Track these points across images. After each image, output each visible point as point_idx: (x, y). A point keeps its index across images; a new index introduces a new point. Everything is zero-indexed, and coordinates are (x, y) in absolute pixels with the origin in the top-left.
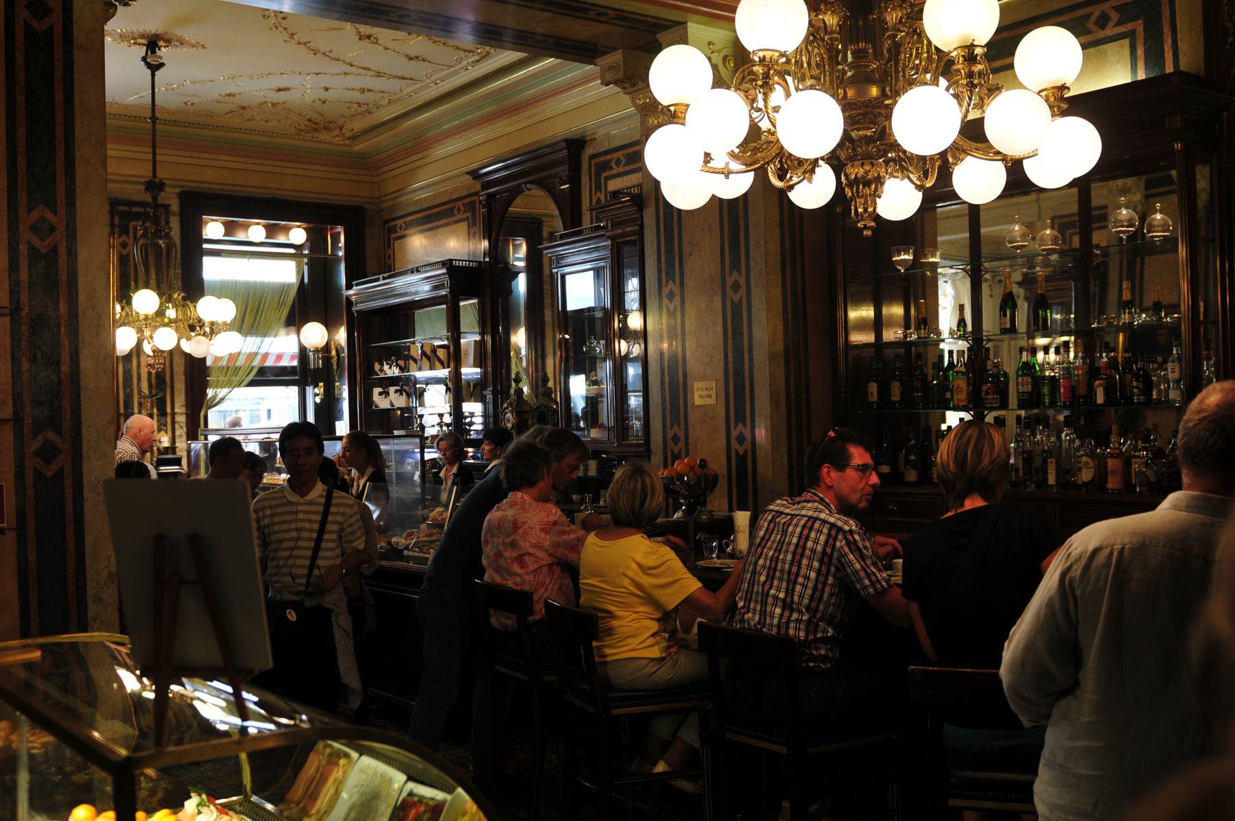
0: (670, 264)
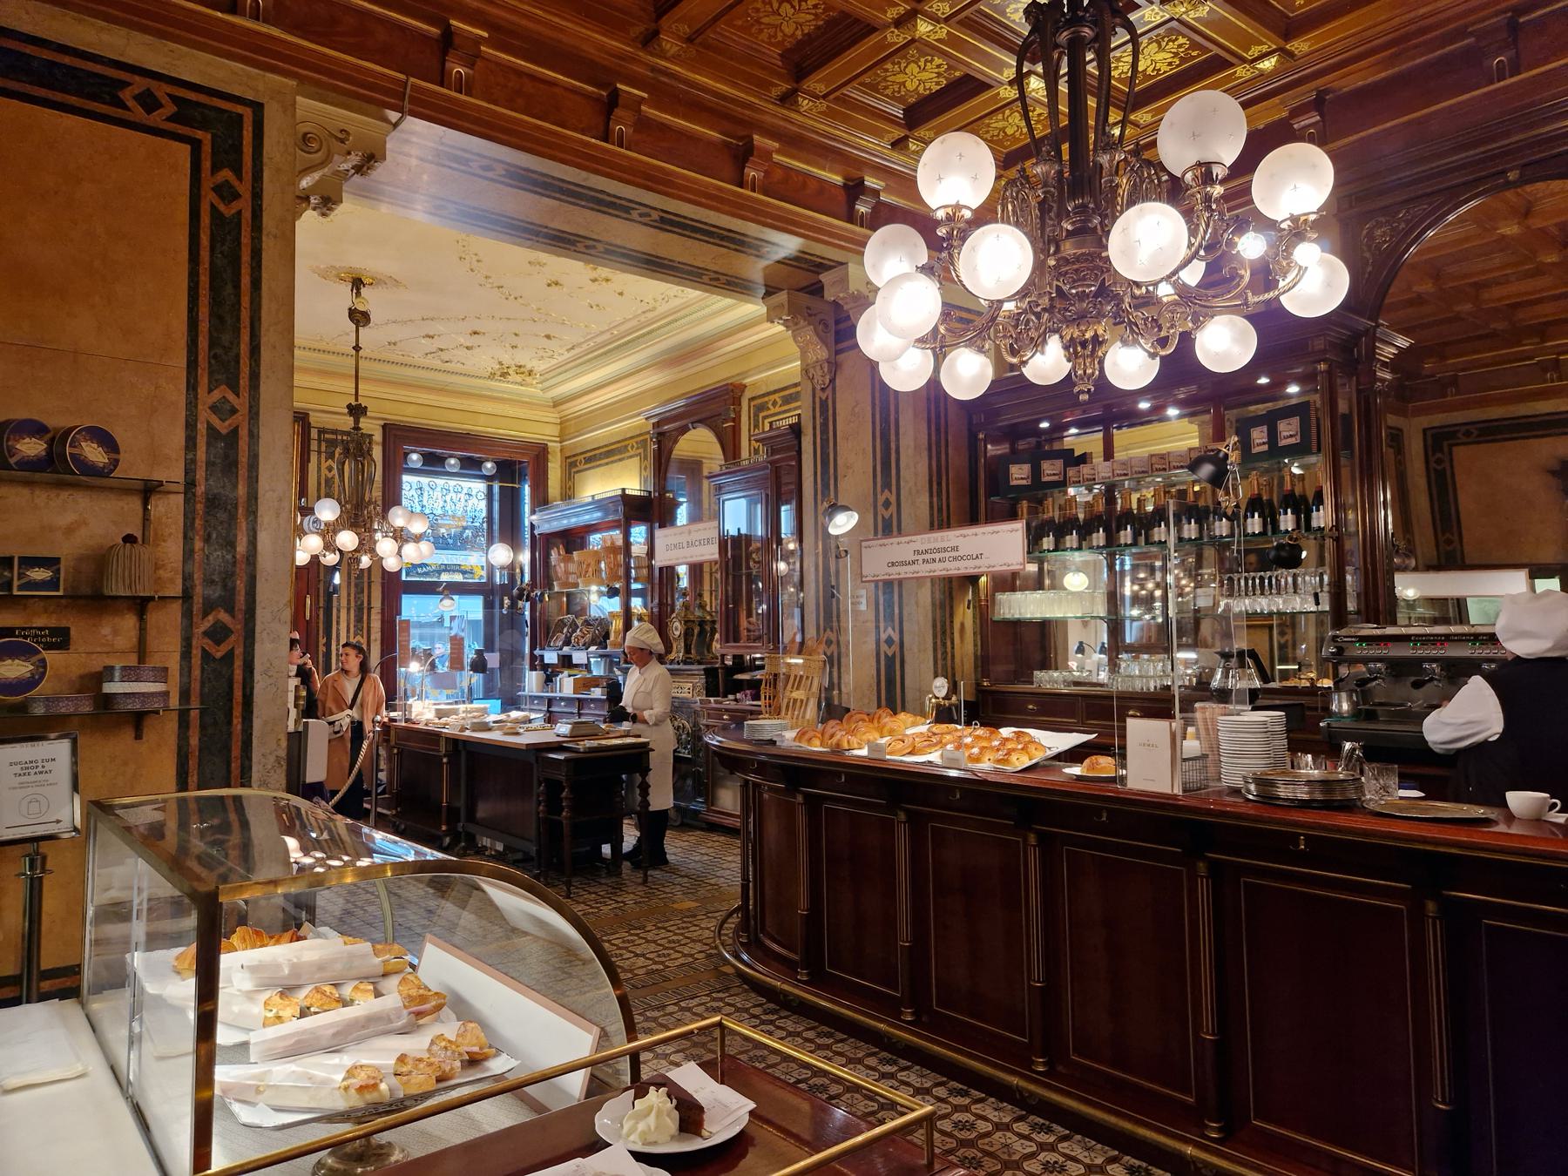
0: (826, 486)
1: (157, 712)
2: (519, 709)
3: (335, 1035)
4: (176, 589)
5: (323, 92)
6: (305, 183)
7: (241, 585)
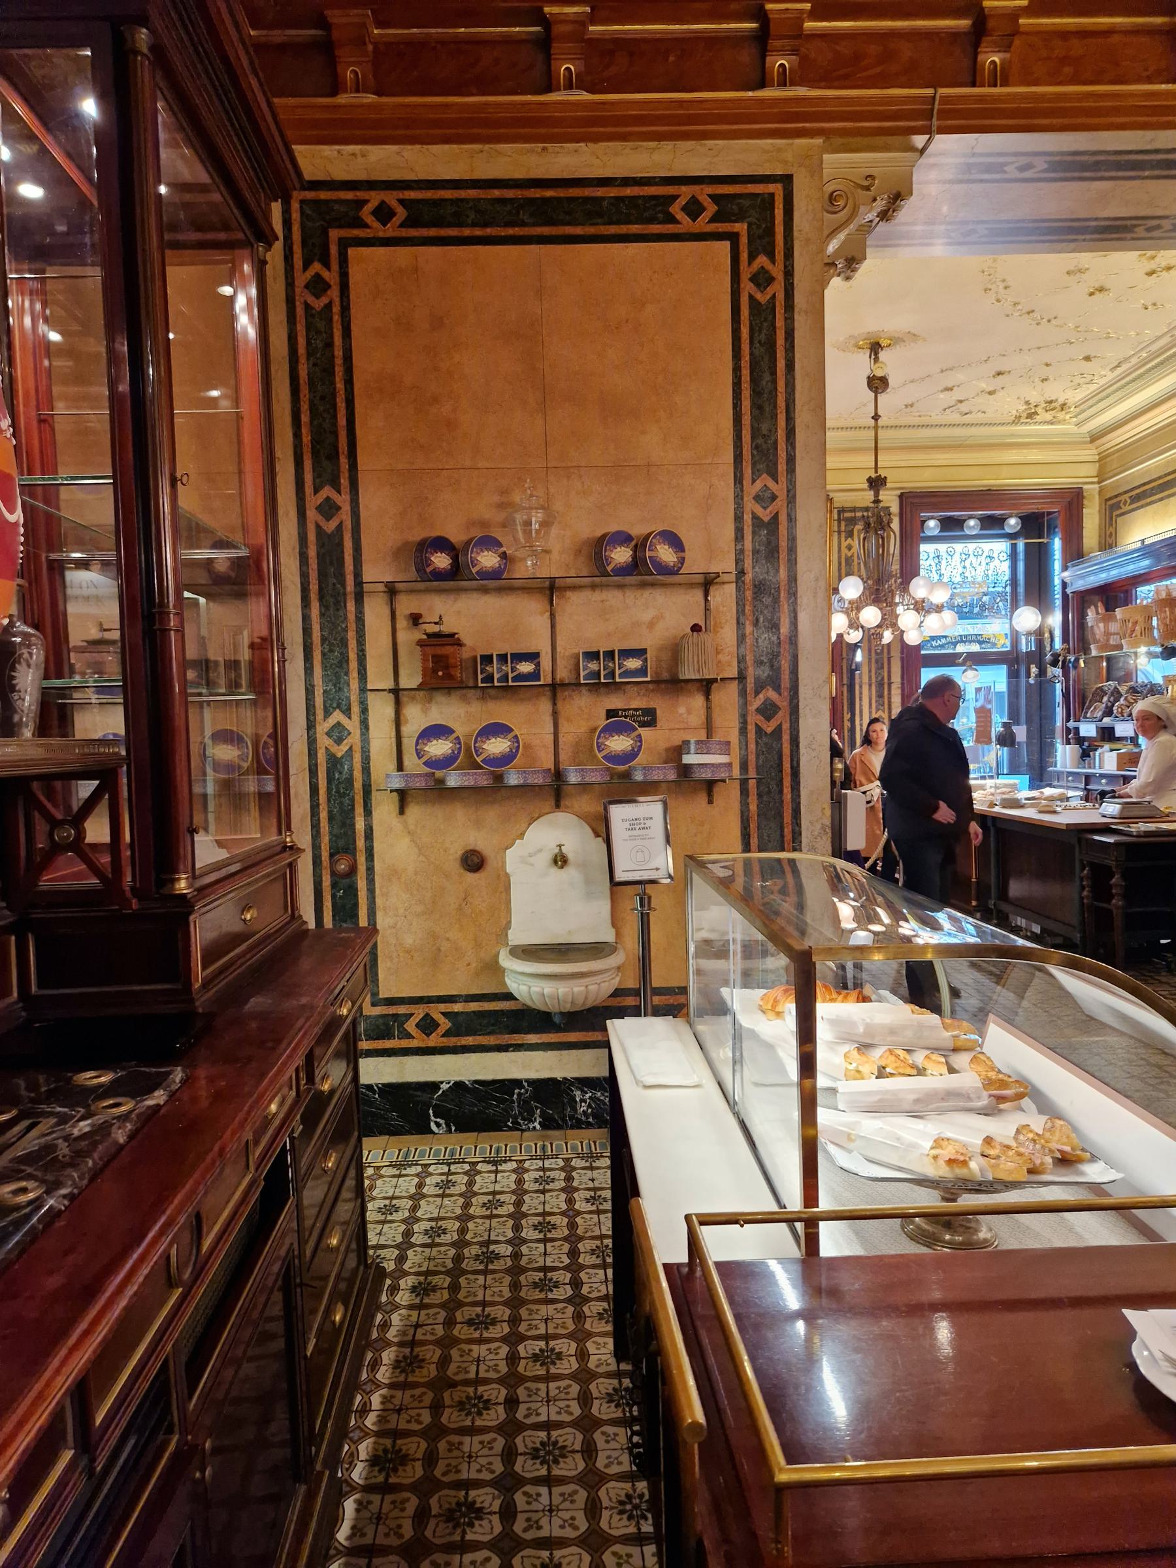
1: (724, 781)
2: (1050, 786)
3: (917, 1101)
4: (733, 672)
5: (849, 140)
6: (832, 247)
7: (785, 665)
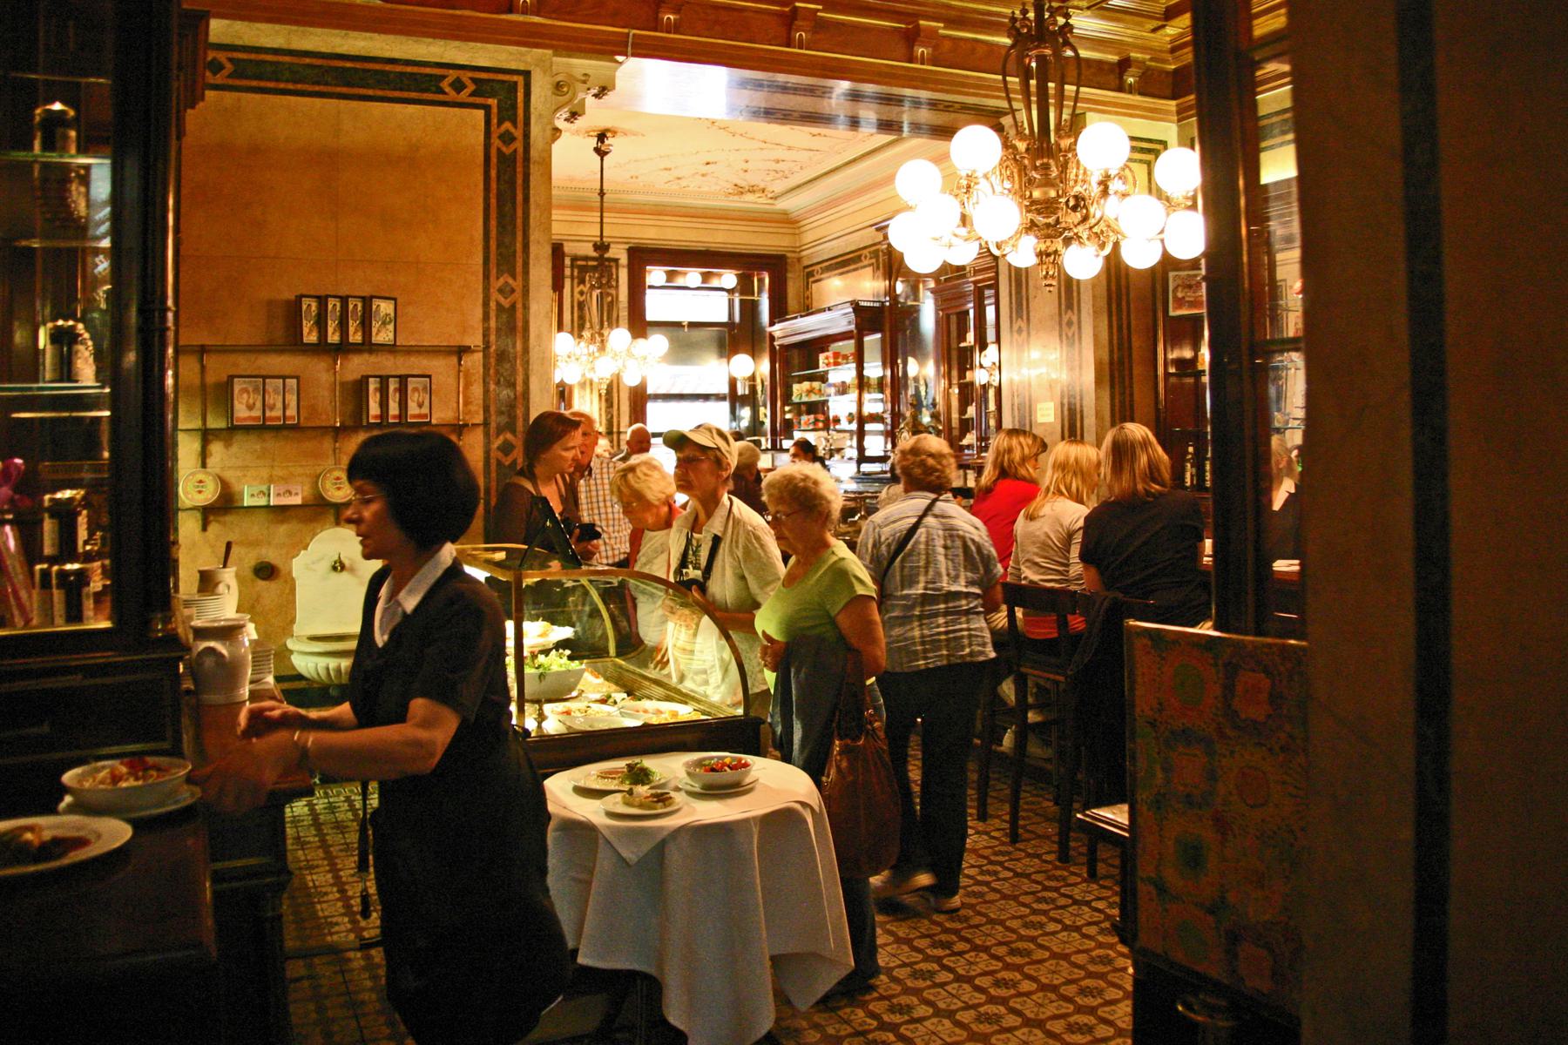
0: (1019, 305)
4: (479, 419)
